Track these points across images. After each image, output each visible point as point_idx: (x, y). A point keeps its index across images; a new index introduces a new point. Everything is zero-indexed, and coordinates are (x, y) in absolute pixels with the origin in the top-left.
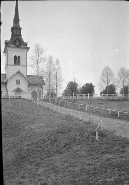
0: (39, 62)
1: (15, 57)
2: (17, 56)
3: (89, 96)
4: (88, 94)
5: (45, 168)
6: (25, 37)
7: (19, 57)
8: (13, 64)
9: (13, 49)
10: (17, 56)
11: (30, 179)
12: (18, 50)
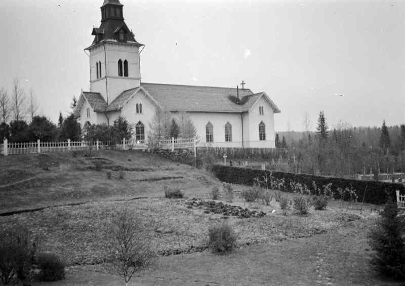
0: (21, 102)
1: (120, 61)
2: (123, 61)
3: (41, 145)
4: (39, 141)
5: (92, 205)
6: (130, 20)
7: (126, 62)
8: (117, 74)
9: (116, 48)
10: (123, 61)
11: (386, 167)
12: (122, 48)
